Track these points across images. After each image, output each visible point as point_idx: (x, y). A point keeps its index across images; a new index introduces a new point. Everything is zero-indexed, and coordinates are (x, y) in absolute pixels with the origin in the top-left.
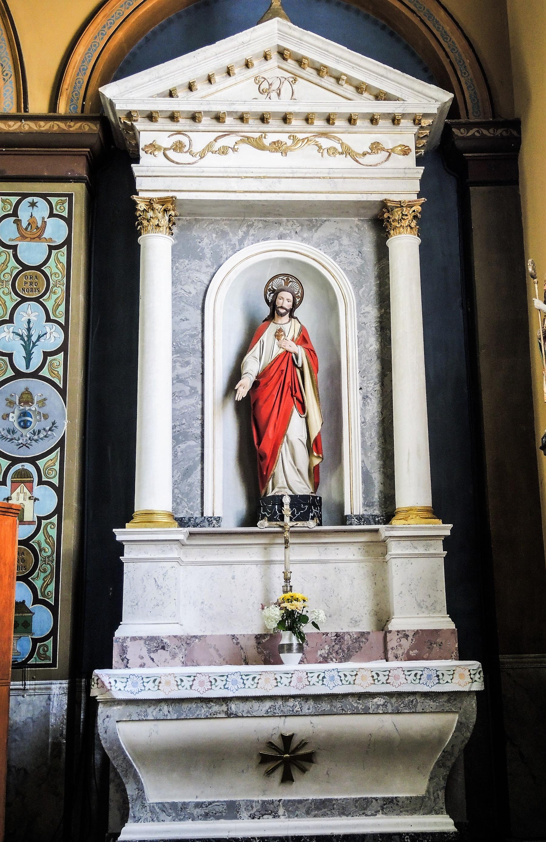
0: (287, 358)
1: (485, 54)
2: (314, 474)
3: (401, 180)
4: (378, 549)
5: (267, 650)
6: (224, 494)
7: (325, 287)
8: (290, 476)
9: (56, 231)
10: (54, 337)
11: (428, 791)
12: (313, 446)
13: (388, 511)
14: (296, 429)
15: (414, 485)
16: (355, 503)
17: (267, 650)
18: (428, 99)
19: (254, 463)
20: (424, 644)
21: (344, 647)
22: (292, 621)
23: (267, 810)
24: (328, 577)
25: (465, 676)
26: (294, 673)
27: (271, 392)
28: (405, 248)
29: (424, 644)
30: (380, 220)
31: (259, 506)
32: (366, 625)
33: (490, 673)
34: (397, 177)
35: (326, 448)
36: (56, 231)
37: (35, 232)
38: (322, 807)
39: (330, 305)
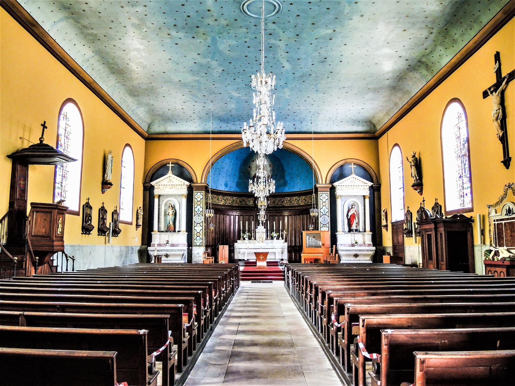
0: (354, 214)
1: (376, 172)
2: (356, 226)
3: (367, 193)
4: (364, 235)
5: (353, 245)
6: (347, 229)
7: (357, 204)
8: (354, 227)
9: (327, 198)
10: (327, 210)
11: (197, 264)
12: (357, 223)
13: (365, 231)
14: (355, 222)
15: (368, 228)
16: (361, 230)
17: (353, 245)
18: (371, 184)
19: (350, 225)
20: (369, 245)
21: (361, 245)
22: (356, 243)
23: (354, 260)
24: (358, 237)
25: (374, 248)
26: (356, 248)
27: (352, 217)
28: (367, 201)
29: (369, 245)
30: (364, 197)
31: (350, 230)
32: (362, 243)
33: (376, 248)
34: (367, 193)
35: (358, 223)
36: (327, 198)
37: (324, 198)
38: (359, 260)
39: (358, 206)
